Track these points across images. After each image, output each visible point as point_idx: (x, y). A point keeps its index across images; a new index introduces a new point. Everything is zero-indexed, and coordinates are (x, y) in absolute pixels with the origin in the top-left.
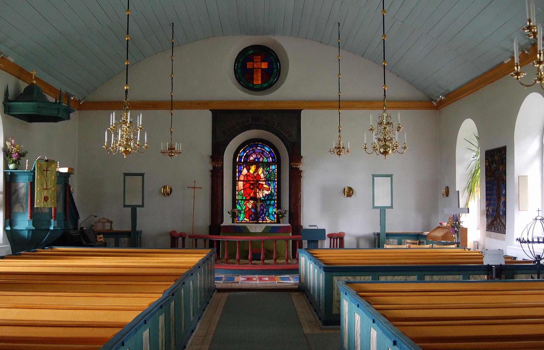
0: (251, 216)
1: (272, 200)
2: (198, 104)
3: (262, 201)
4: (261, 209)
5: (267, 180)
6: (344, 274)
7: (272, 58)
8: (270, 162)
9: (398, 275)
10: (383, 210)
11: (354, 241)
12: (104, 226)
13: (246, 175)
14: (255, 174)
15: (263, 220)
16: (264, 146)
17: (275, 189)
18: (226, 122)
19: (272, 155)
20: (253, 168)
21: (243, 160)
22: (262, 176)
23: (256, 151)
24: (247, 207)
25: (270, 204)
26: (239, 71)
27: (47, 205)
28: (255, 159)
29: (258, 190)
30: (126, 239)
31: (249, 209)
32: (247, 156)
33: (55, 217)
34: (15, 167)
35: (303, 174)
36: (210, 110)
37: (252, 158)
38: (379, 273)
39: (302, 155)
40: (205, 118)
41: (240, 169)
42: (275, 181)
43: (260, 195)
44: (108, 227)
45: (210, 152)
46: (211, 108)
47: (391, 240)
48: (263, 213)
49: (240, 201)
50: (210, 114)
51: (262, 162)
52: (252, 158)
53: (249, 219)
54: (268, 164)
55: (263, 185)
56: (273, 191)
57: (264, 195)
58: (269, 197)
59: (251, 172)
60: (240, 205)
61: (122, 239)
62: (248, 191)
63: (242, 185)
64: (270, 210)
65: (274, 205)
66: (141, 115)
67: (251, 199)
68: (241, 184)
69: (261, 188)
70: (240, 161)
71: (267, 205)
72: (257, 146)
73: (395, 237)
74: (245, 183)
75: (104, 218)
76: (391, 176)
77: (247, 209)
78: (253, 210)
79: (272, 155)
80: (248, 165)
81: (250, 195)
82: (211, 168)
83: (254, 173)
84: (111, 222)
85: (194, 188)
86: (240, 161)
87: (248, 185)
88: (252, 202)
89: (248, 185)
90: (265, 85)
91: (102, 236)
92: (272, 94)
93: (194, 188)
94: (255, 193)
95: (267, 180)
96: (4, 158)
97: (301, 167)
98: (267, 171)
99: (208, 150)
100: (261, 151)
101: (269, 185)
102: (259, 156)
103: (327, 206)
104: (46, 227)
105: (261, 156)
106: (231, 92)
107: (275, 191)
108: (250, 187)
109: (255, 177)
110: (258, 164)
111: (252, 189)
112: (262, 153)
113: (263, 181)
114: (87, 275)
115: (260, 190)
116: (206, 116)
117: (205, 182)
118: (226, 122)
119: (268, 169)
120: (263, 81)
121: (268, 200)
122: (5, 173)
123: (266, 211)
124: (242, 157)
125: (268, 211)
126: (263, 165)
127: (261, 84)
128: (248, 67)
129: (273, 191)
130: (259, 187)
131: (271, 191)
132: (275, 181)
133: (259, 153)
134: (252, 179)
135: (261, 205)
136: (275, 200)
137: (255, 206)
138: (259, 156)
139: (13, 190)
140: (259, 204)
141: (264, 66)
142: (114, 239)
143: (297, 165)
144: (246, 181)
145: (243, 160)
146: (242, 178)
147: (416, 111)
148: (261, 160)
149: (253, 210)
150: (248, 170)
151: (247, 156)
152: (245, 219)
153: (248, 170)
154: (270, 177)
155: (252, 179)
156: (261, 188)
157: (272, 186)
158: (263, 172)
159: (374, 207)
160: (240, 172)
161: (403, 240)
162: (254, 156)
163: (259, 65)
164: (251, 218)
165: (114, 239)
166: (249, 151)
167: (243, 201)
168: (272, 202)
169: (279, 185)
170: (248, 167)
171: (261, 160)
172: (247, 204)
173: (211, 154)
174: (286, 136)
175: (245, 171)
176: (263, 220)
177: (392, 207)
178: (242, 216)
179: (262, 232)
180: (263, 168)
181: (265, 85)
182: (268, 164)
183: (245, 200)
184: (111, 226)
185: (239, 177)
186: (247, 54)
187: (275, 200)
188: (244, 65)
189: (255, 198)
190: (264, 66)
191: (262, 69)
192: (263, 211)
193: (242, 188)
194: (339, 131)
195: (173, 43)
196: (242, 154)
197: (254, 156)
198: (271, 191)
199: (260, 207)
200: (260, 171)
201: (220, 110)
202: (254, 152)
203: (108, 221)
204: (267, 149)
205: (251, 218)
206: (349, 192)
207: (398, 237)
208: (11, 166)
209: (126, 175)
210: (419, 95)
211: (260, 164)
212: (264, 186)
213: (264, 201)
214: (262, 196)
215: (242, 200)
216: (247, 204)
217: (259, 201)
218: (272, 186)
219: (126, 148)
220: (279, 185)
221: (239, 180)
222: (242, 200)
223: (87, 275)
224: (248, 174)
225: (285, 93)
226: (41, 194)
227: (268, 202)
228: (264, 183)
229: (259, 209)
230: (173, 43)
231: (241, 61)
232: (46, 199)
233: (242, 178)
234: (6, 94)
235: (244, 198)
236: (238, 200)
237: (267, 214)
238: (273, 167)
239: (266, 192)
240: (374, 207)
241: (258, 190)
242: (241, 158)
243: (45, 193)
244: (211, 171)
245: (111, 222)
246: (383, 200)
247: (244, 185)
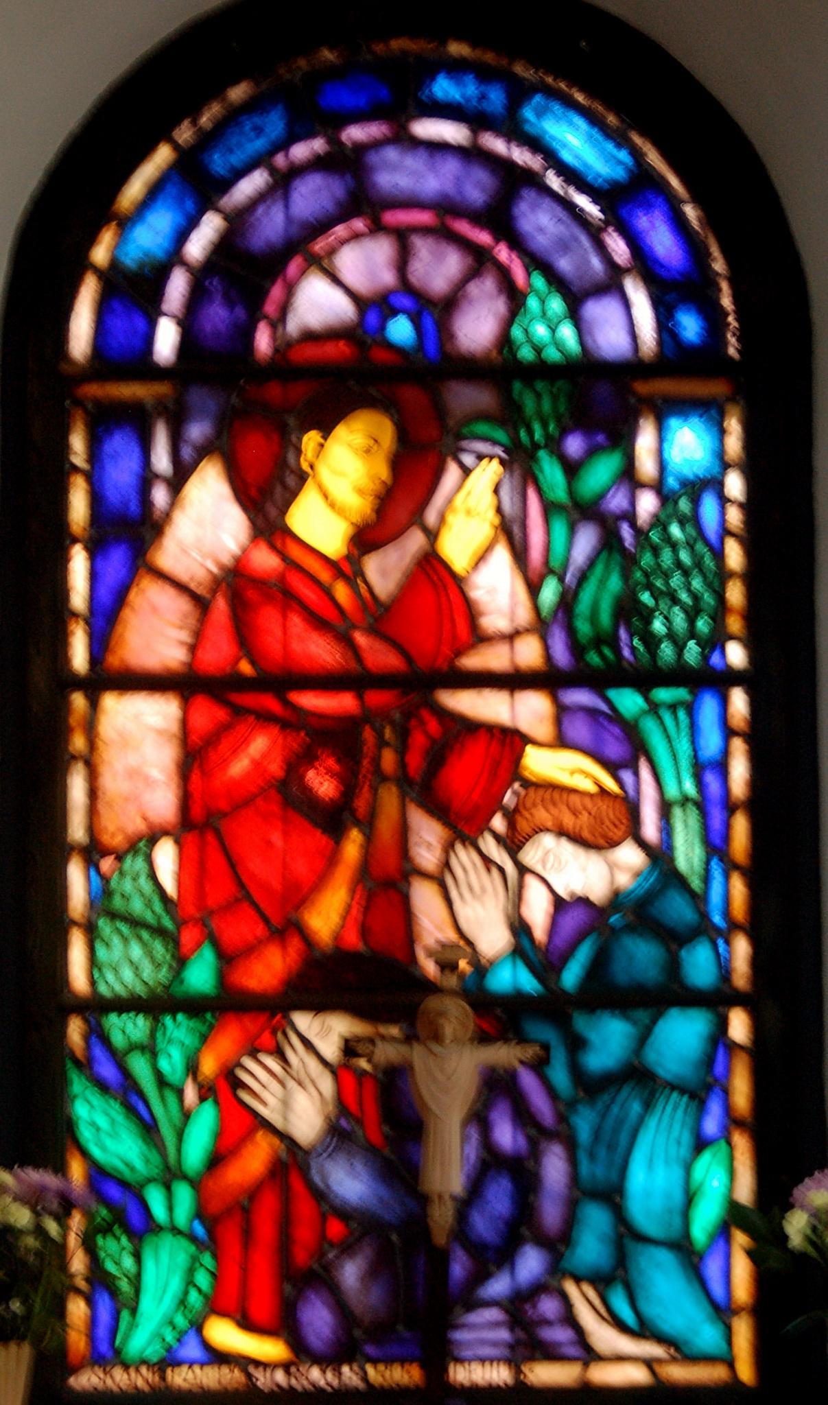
0: (321, 1279)
1: (673, 993)
3: (499, 1016)
4: (492, 1161)
5: (593, 666)
8: (631, 369)
13: (236, 581)
14: (385, 572)
15: (528, 1344)
16: (518, 94)
17: (711, 807)
19: (663, 242)
20: (342, 471)
21: (166, 340)
22: (497, 591)
23: (398, 173)
24: (241, 1124)
25: (637, 1076)
28: (375, 307)
29: (427, 839)
31: (292, 1160)
32: (248, 273)
37: (318, 303)
41: (121, 474)
43: (475, 911)
48: (522, 1226)
49: (126, 1029)
51: (504, 369)
52: (318, 303)
53: (282, 1324)
54: (604, 400)
55: (512, 741)
56: (688, 853)
57: (537, 910)
58: (608, 963)
60: (127, 1093)
62: (270, 849)
64: (649, 1181)
65: (702, 1088)
67: (329, 980)
69: (474, 786)
70: (122, 355)
71: (592, 1087)
72: (402, 102)
74: (207, 715)
77: (255, 1160)
78: (350, 1183)
79: (663, 242)
80: (258, 407)
81: (289, 927)
83: (366, 538)
86: (122, 355)
87: (255, 753)
88: (328, 1032)
89: (255, 753)
94: (387, 887)
95: (593, 666)
98: (584, 511)
100: (477, 188)
101: (625, 749)
102: (438, 268)
105: (480, 260)
107: (716, 847)
108: (288, 791)
109: (381, 616)
110: (422, 394)
111: (332, 820)
112: (499, 217)
113: (514, 681)
114: (671, 746)
115: (463, 828)
121: (603, 993)
123: (579, 1192)
124: (157, 274)
125: (612, 1195)
126: (509, 416)
129: (688, 853)
130: (461, 775)
131: (660, 855)
133: (447, 207)
134: (321, 651)
135: (498, 1087)
136: (718, 1000)
137: (381, 1113)
138: (438, 268)
140: (451, 1075)
146: (157, 632)
148: (476, 328)
149: (350, 1183)
150: (266, 494)
152: (225, 1334)
153: (266, 494)
154: (629, 611)
155: (321, 651)
156: (474, 786)
157: (669, 773)
158: (511, 532)
162: (364, 261)
164: (318, 1319)
166: (283, 182)
167: (179, 1033)
168: (680, 1037)
171: (476, 328)
172: (260, 1075)
175: (206, 523)
176: (528, 1344)
178: (164, 1279)
180: (520, 462)
182: (604, 400)
183: (223, 1005)
185: (105, 619)
187: (718, 1000)
189: (378, 978)
192: (523, 1174)
193: (163, 802)
196: (151, 236)
197: (364, 261)
198: (660, 855)
199: (479, 1119)
200: (470, 506)
202: (364, 205)
204: (573, 138)
205: (318, 1319)
211: (468, 397)
212: (541, 762)
213: (553, 1011)
214: (492, 938)
215: (157, 1005)
216: (260, 1075)
217: (455, 1016)
218: (669, 773)
219: (384, 778)
221: (112, 678)
222: (157, 1005)
223: (671, 746)
224: (265, 560)
227: (609, 1040)
228: (530, 711)
229: (449, 1167)
233: (157, 632)
235: (201, 975)
236: (97, 1007)
237: (591, 1246)
238: (686, 445)
239: (575, 871)
241: (427, 839)
242: (134, 292)
247: (194, 756)
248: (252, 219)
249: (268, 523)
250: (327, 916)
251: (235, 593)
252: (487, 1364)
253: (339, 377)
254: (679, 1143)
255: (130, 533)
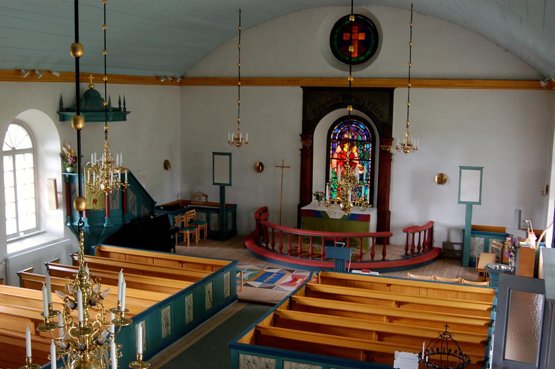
2: (289, 81)
5: (362, 159)
6: (249, 353)
7: (369, 28)
8: (365, 141)
9: (303, 363)
10: (469, 205)
11: (445, 232)
12: (200, 199)
13: (340, 153)
16: (359, 123)
17: (368, 169)
18: (317, 99)
20: (347, 146)
21: (337, 137)
22: (356, 154)
23: (351, 128)
26: (335, 43)
27: (97, 207)
30: (216, 215)
32: (342, 134)
33: (108, 215)
34: (71, 170)
35: (393, 157)
36: (301, 87)
38: (284, 358)
39: (393, 137)
40: (296, 95)
41: (334, 146)
42: (369, 161)
44: (203, 199)
45: (300, 131)
46: (302, 85)
47: (477, 238)
50: (300, 91)
51: (357, 141)
55: (356, 164)
59: (345, 150)
61: (213, 215)
63: (335, 164)
66: (121, 155)
68: (334, 162)
70: (334, 138)
72: (352, 123)
73: (482, 236)
74: (338, 161)
75: (199, 192)
76: (481, 169)
80: (343, 142)
82: (301, 147)
84: (207, 196)
85: (283, 167)
86: (334, 138)
90: (362, 58)
91: (194, 210)
92: (361, 71)
93: (283, 167)
96: (62, 162)
97: (393, 150)
98: (361, 150)
99: (299, 129)
101: (363, 165)
103: (418, 194)
104: (100, 224)
105: (356, 134)
106: (323, 67)
110: (352, 143)
113: (357, 160)
116: (297, 93)
117: (294, 160)
118: (317, 99)
119: (362, 148)
120: (360, 54)
122: (64, 176)
127: (358, 57)
128: (344, 39)
132: (369, 161)
139: (72, 190)
141: (362, 37)
142: (205, 214)
143: (387, 148)
144: (339, 159)
145: (337, 137)
146: (336, 156)
147: (525, 91)
150: (342, 148)
151: (342, 134)
153: (342, 148)
154: (364, 156)
157: (365, 167)
158: (357, 151)
159: (460, 202)
160: (334, 149)
161: (491, 239)
163: (355, 37)
165: (205, 214)
166: (344, 128)
169: (373, 165)
170: (342, 144)
173: (301, 133)
174: (377, 116)
175: (339, 149)
177: (479, 203)
179: (342, 219)
180: (358, 147)
181: (362, 58)
182: (363, 143)
184: (206, 199)
185: (332, 155)
186: (343, 24)
188: (340, 36)
190: (362, 37)
191: (359, 41)
194: (407, 126)
195: (240, 31)
196: (336, 131)
201: (311, 87)
203: (204, 195)
204: (362, 126)
206: (442, 180)
207: (484, 236)
208: (68, 169)
209: (214, 154)
210: (530, 73)
211: (355, 143)
219: (106, 187)
220: (373, 165)
225: (384, 66)
226: (90, 197)
228: (358, 162)
230: (240, 31)
231: (337, 32)
232: (95, 201)
233: (336, 156)
234: (61, 103)
240: (460, 202)
242: (335, 135)
243: (94, 196)
244: (301, 150)
245: (207, 196)
246: (470, 194)
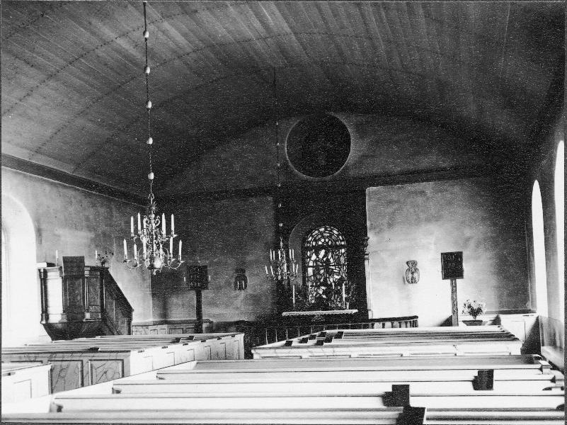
20: (322, 253)
83: (323, 258)
88: (323, 288)
95: (338, 264)
112: (331, 237)
150: (317, 255)
153: (317, 255)
162: (323, 240)
175: (314, 257)
183: (316, 286)
204: (335, 232)
228: (334, 267)
247: (314, 271)
248: (275, 30)
249: (318, 257)
250: (322, 280)
251: (315, 261)
252: (173, 37)
253: (322, 247)
254: (219, 338)
255: (310, 257)
